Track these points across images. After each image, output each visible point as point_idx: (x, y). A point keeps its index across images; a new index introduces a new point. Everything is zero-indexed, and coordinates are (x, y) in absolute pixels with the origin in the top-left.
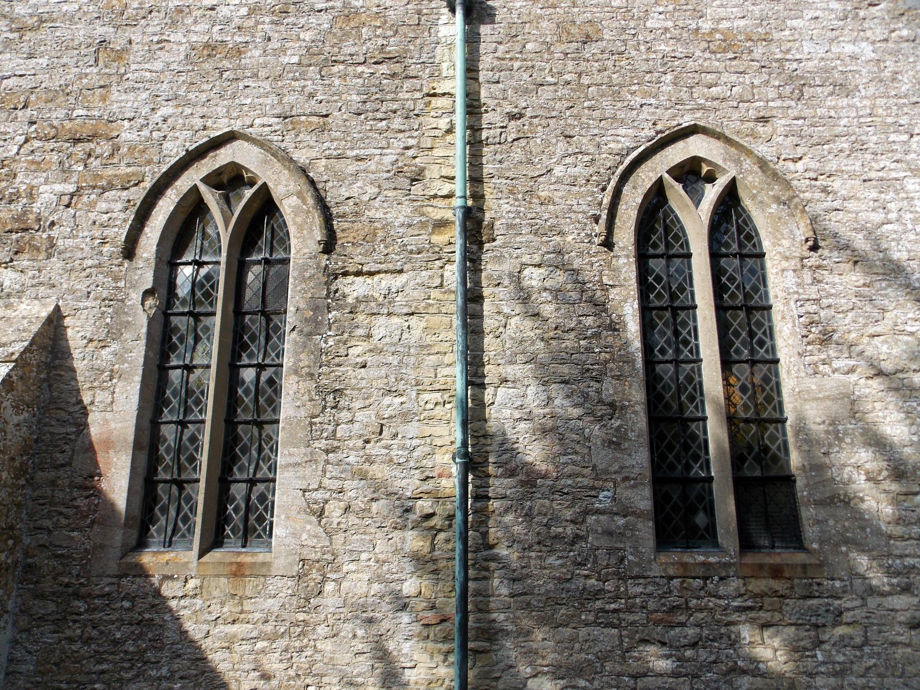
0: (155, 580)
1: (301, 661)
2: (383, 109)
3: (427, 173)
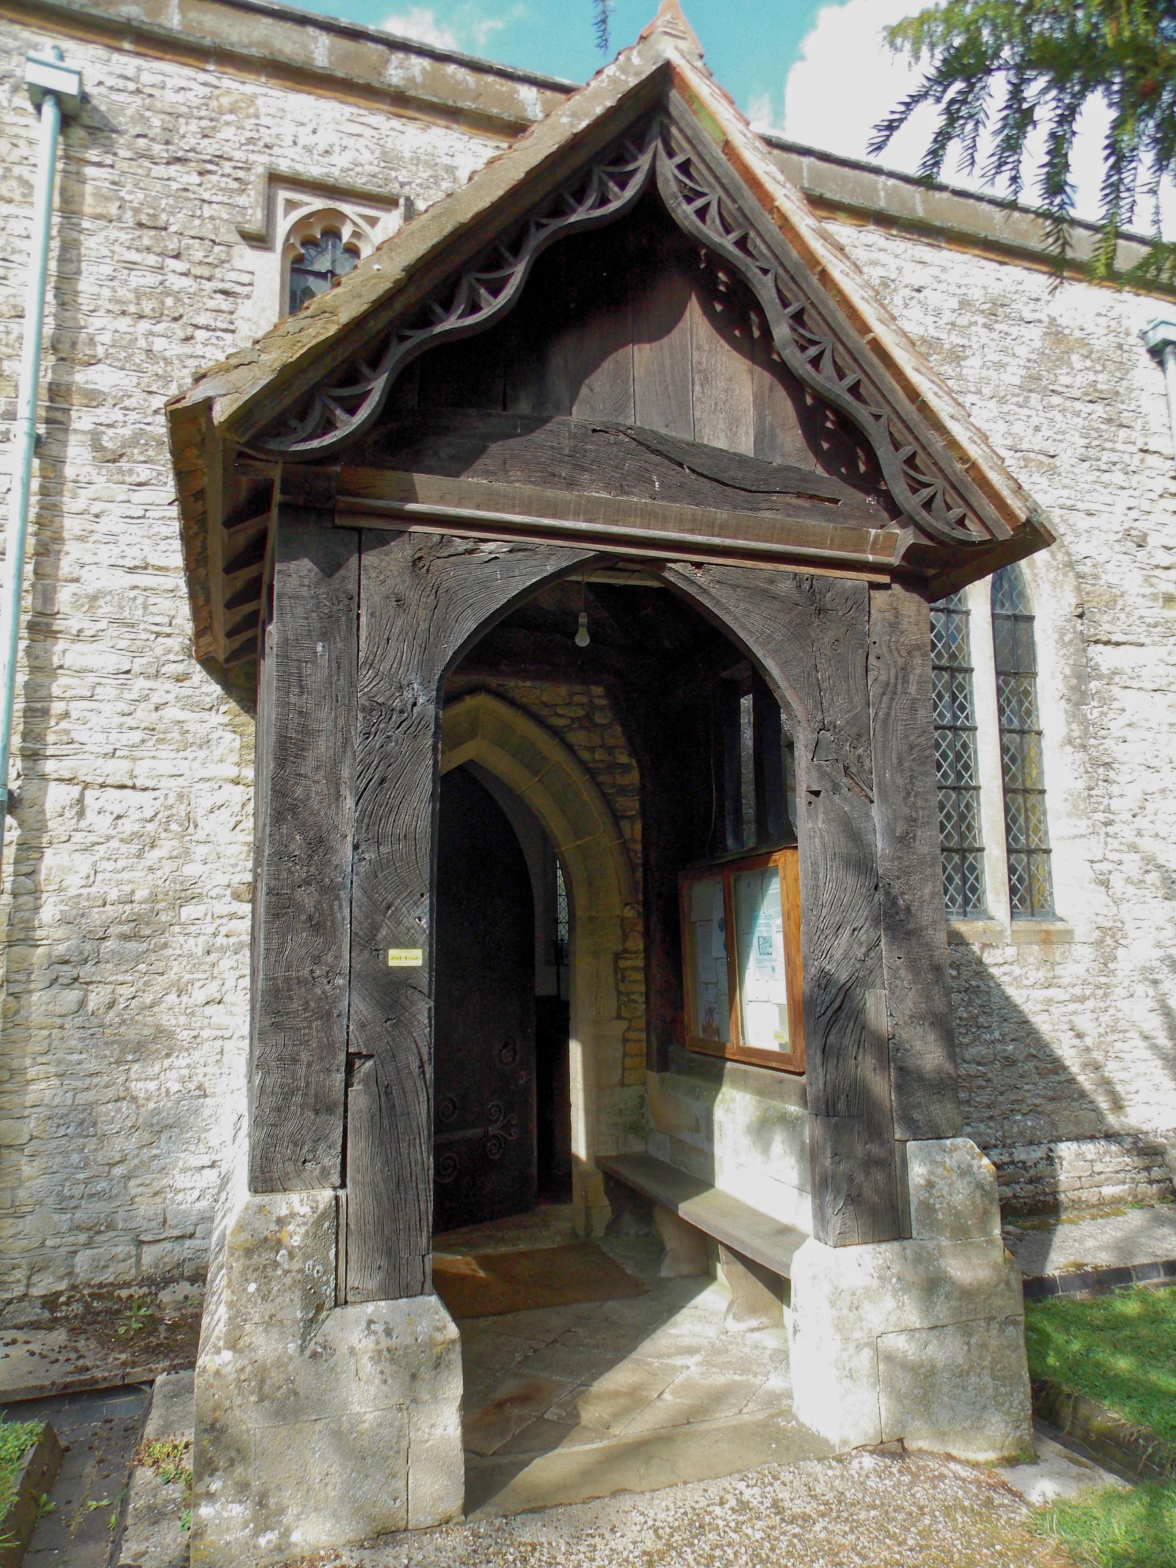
0: (976, 948)
1: (1105, 1018)
2: (1104, 459)
3: (1149, 539)
